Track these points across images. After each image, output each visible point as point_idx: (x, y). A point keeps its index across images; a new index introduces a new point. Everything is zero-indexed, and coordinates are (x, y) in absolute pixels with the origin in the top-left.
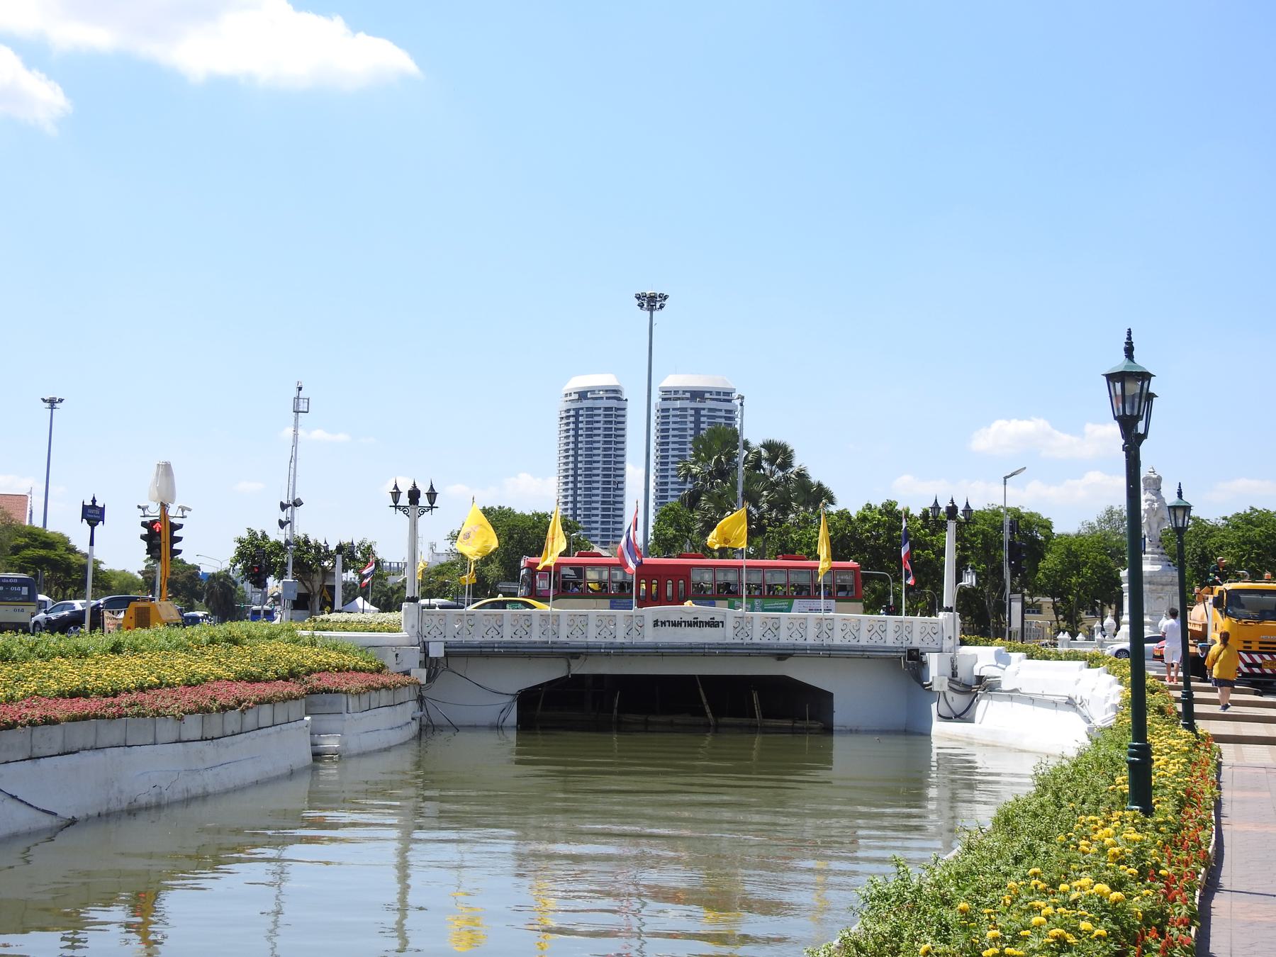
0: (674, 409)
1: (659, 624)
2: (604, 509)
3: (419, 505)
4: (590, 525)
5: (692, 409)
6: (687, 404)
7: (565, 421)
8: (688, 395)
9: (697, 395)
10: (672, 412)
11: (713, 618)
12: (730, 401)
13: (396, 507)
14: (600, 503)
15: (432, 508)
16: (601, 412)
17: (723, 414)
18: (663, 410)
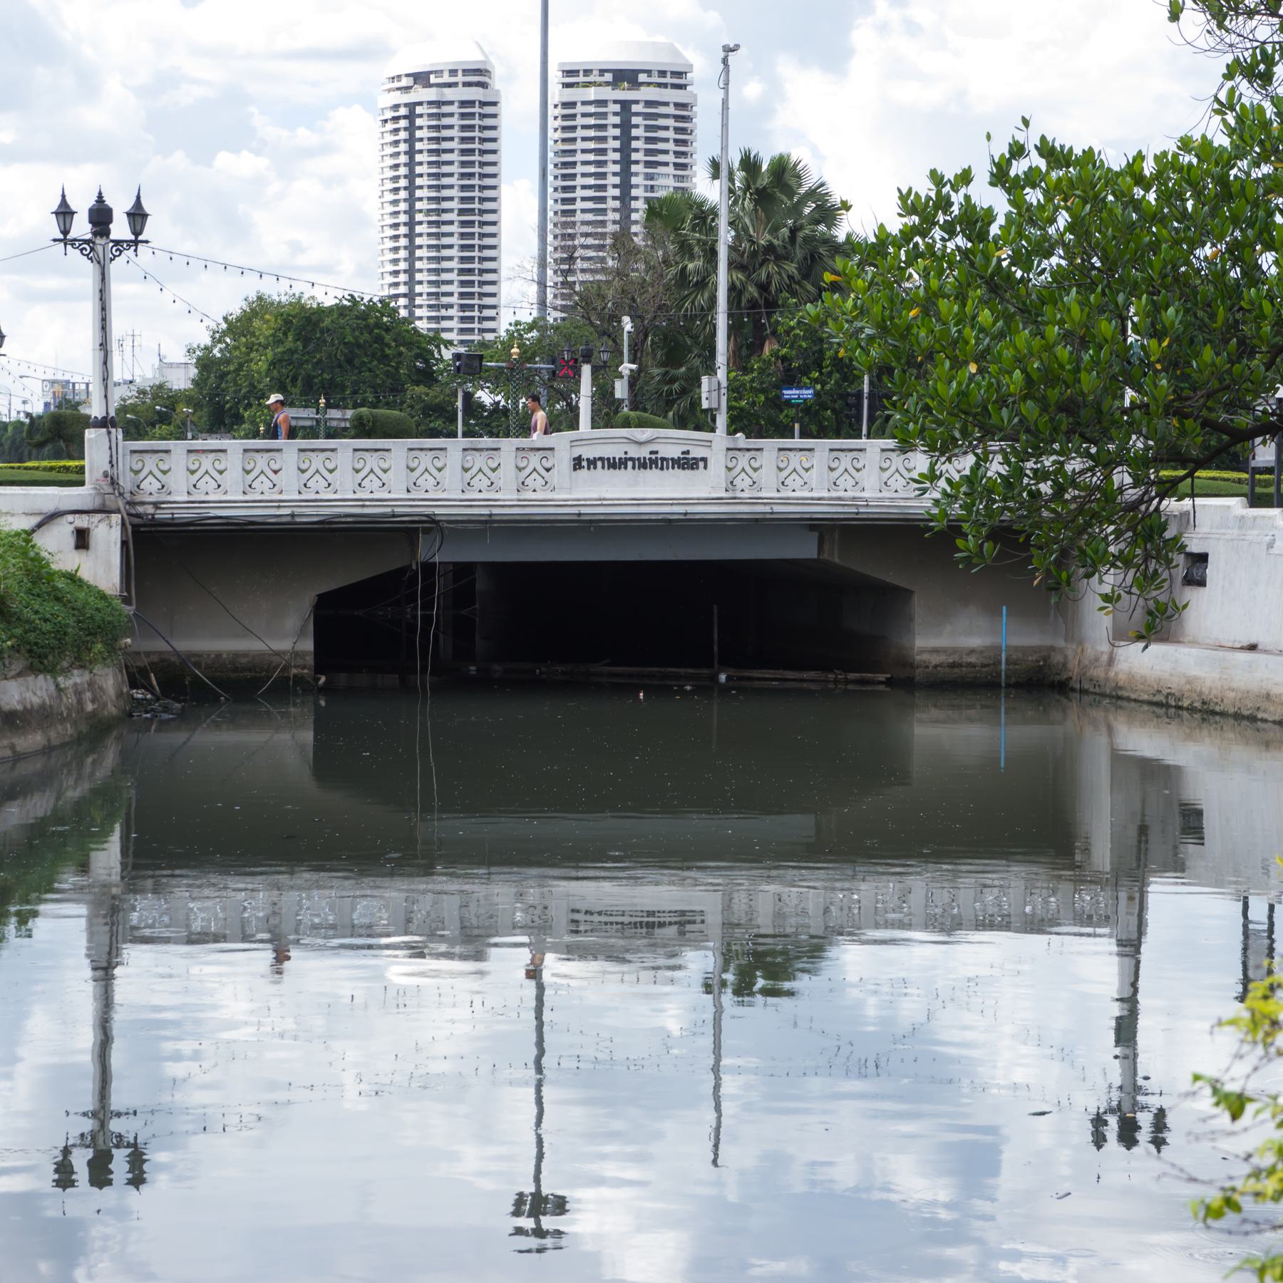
0: (584, 103)
1: (585, 463)
2: (463, 283)
3: (112, 237)
4: (439, 156)
5: (615, 102)
6: (608, 93)
7: (390, 126)
8: (608, 77)
9: (625, 77)
10: (580, 109)
11: (688, 452)
12: (681, 87)
13: (65, 241)
14: (456, 272)
15: (136, 243)
16: (454, 109)
17: (671, 110)
18: (566, 105)
